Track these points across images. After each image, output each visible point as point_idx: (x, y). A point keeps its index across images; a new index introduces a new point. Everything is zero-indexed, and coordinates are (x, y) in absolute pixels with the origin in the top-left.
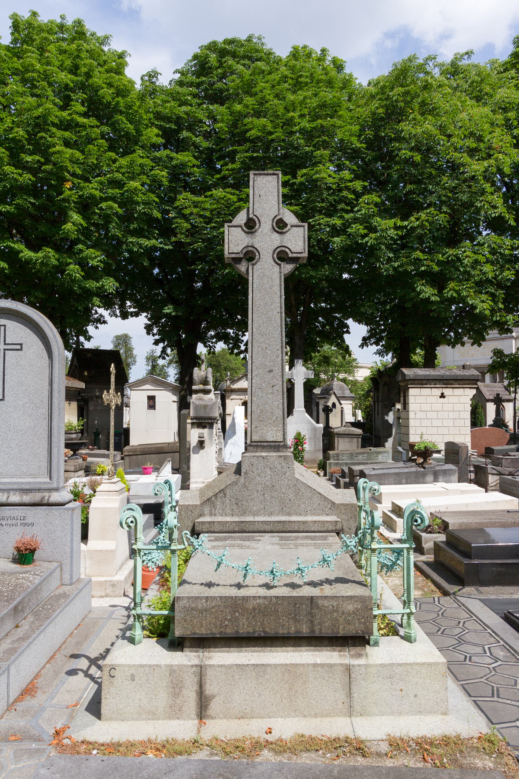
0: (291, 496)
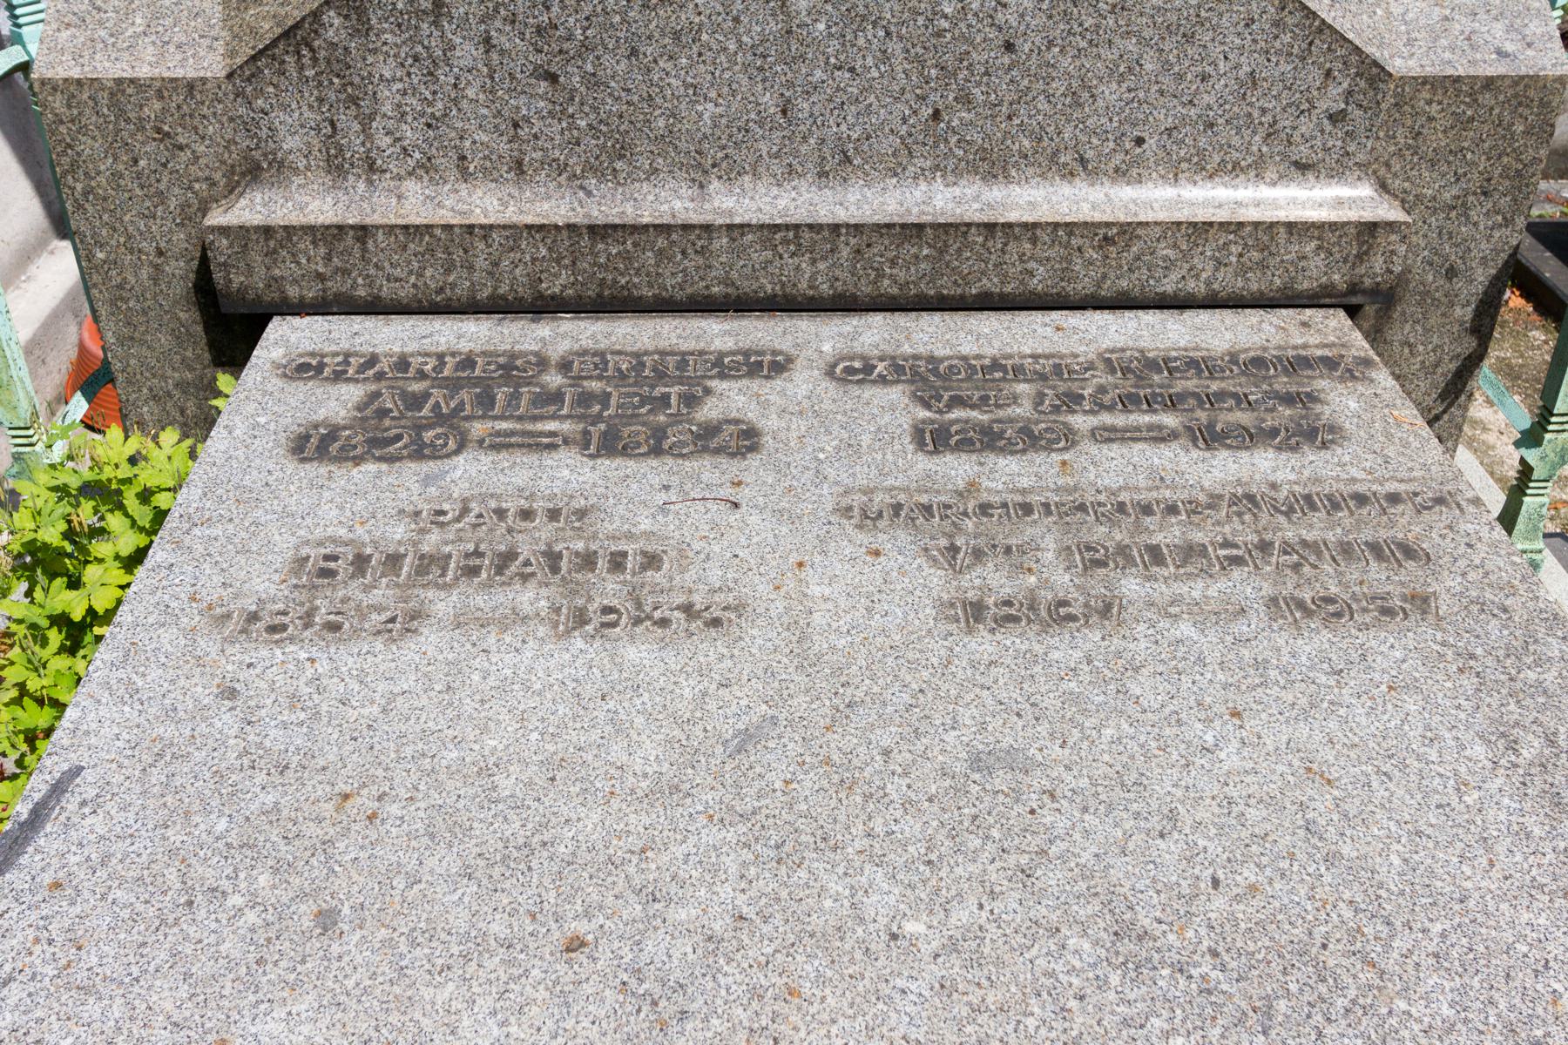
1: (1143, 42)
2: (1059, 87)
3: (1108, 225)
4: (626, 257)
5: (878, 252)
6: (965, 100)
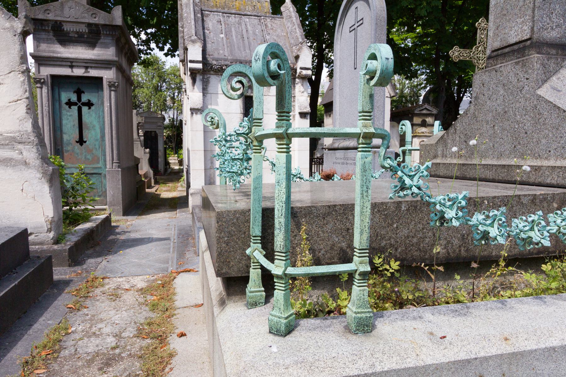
0: (528, 126)
1: (549, 131)
2: (535, 140)
3: (536, 166)
4: (466, 169)
5: (499, 170)
6: (519, 143)
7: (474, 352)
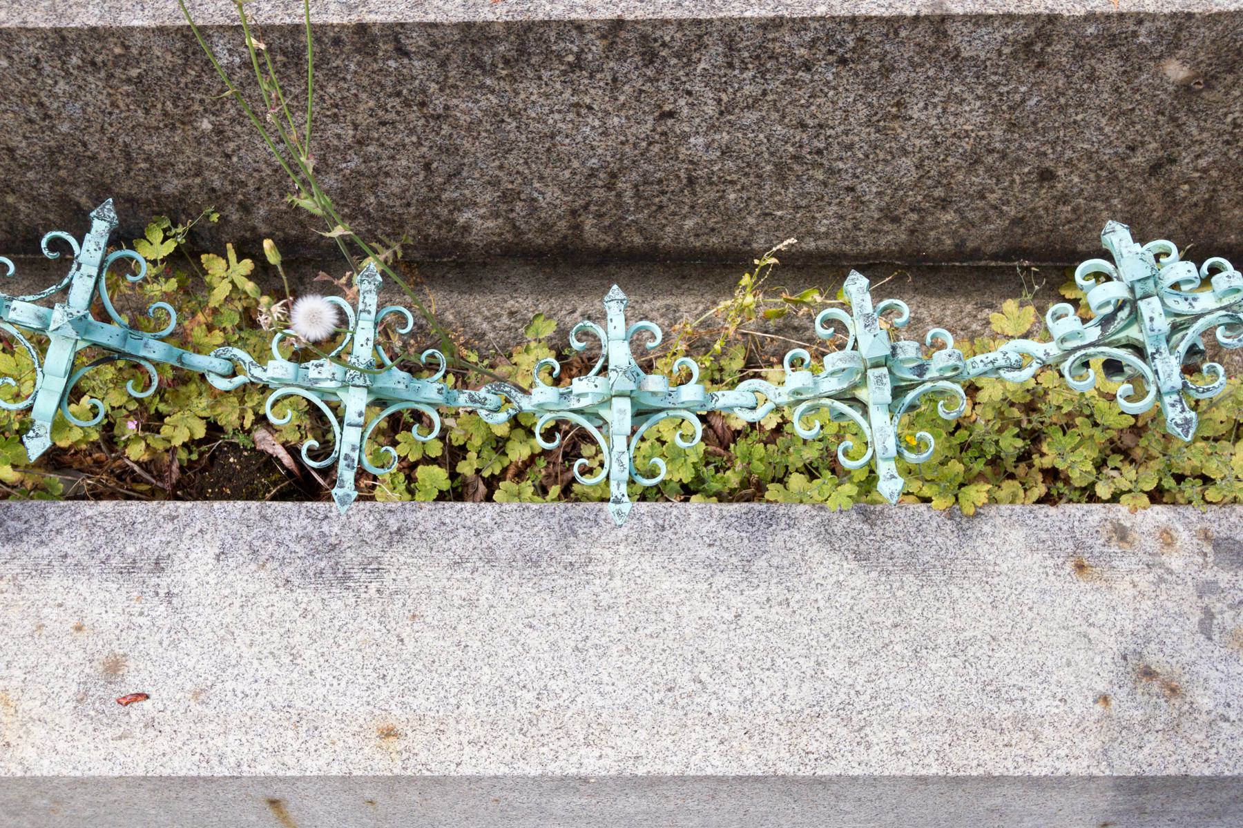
7: (232, 761)
